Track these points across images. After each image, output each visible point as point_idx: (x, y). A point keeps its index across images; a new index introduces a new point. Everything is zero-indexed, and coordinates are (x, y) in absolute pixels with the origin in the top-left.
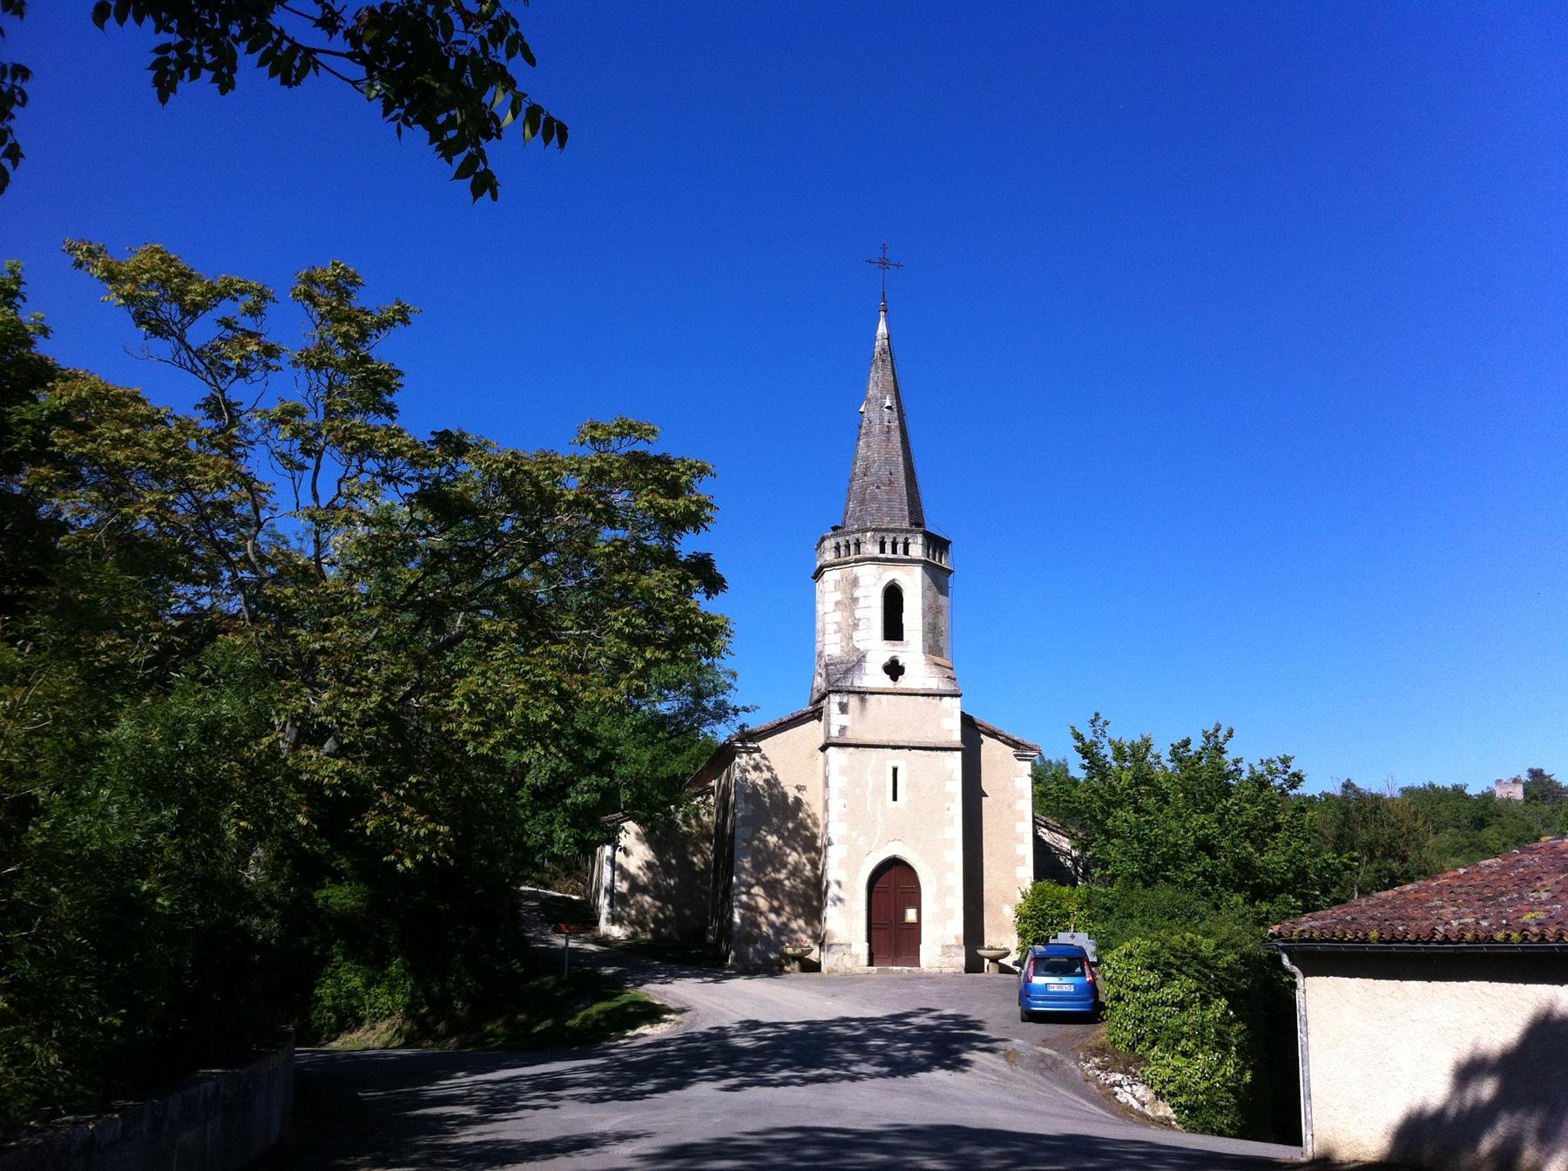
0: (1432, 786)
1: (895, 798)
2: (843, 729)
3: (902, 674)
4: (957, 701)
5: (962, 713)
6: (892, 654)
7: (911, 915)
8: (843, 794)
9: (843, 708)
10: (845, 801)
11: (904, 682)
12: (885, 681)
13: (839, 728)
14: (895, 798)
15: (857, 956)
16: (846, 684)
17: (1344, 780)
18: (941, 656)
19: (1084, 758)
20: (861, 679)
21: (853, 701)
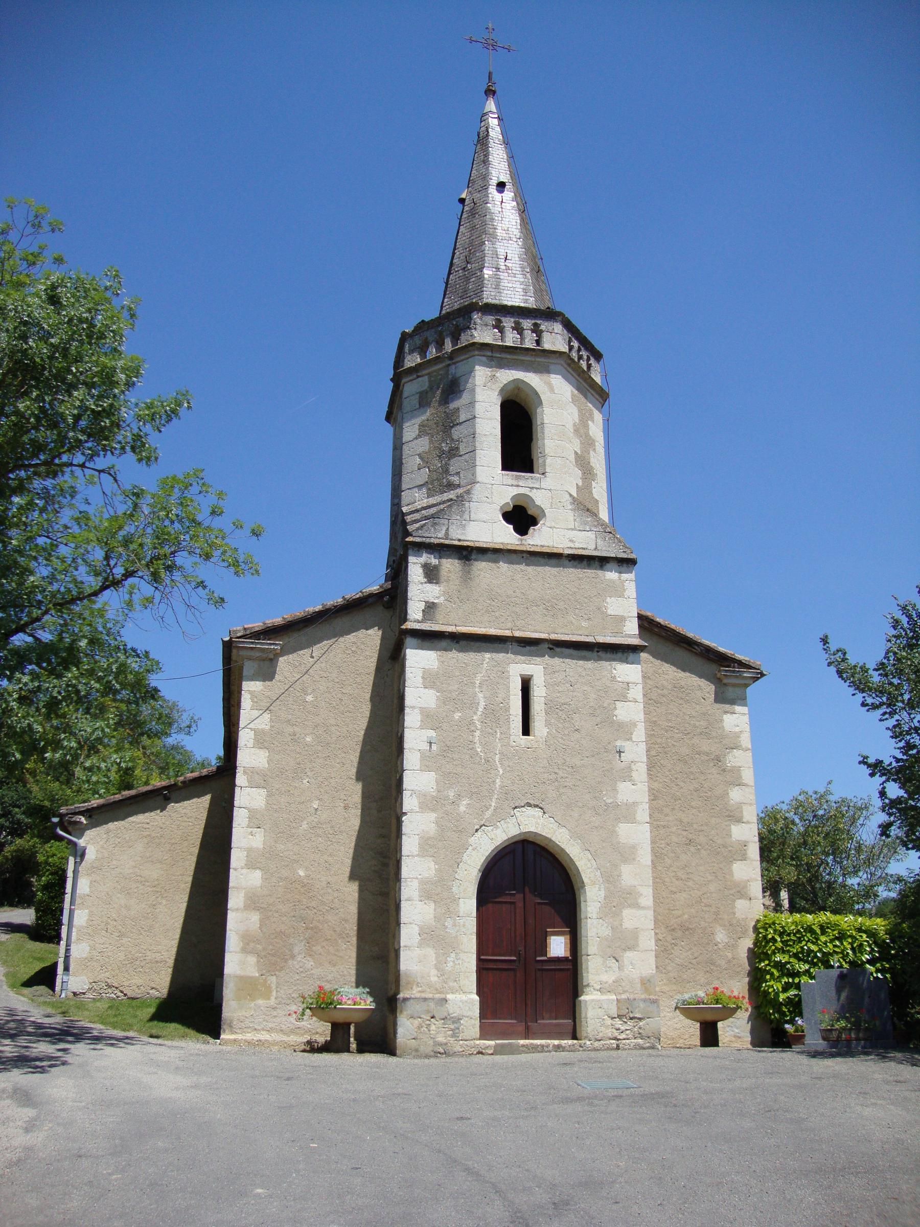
0: (392, 380)
1: (526, 731)
2: (430, 608)
3: (516, 530)
4: (628, 580)
5: (640, 617)
6: (515, 491)
7: (558, 946)
8: (429, 720)
9: (431, 574)
10: (432, 733)
11: (538, 539)
12: (506, 535)
13: (422, 606)
14: (526, 731)
15: (457, 1020)
16: (437, 536)
17: (65, 259)
18: (55, 965)
19: (881, 666)
20: (464, 527)
21: (450, 566)
